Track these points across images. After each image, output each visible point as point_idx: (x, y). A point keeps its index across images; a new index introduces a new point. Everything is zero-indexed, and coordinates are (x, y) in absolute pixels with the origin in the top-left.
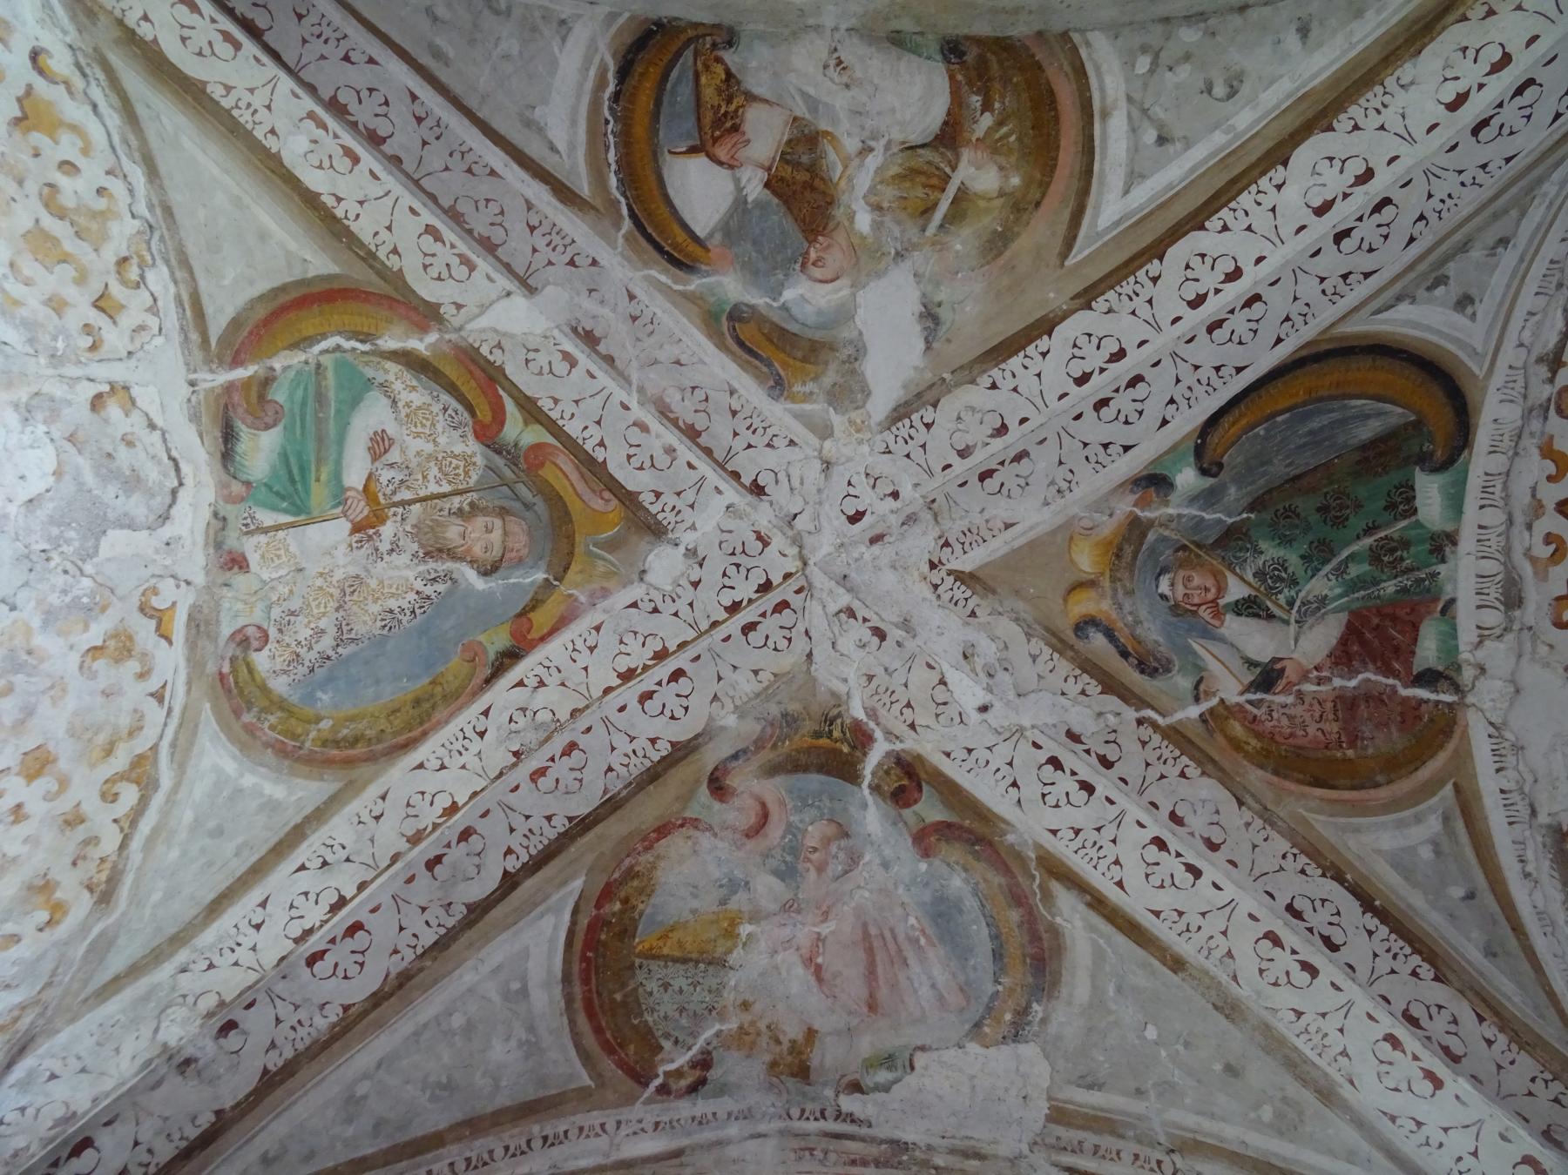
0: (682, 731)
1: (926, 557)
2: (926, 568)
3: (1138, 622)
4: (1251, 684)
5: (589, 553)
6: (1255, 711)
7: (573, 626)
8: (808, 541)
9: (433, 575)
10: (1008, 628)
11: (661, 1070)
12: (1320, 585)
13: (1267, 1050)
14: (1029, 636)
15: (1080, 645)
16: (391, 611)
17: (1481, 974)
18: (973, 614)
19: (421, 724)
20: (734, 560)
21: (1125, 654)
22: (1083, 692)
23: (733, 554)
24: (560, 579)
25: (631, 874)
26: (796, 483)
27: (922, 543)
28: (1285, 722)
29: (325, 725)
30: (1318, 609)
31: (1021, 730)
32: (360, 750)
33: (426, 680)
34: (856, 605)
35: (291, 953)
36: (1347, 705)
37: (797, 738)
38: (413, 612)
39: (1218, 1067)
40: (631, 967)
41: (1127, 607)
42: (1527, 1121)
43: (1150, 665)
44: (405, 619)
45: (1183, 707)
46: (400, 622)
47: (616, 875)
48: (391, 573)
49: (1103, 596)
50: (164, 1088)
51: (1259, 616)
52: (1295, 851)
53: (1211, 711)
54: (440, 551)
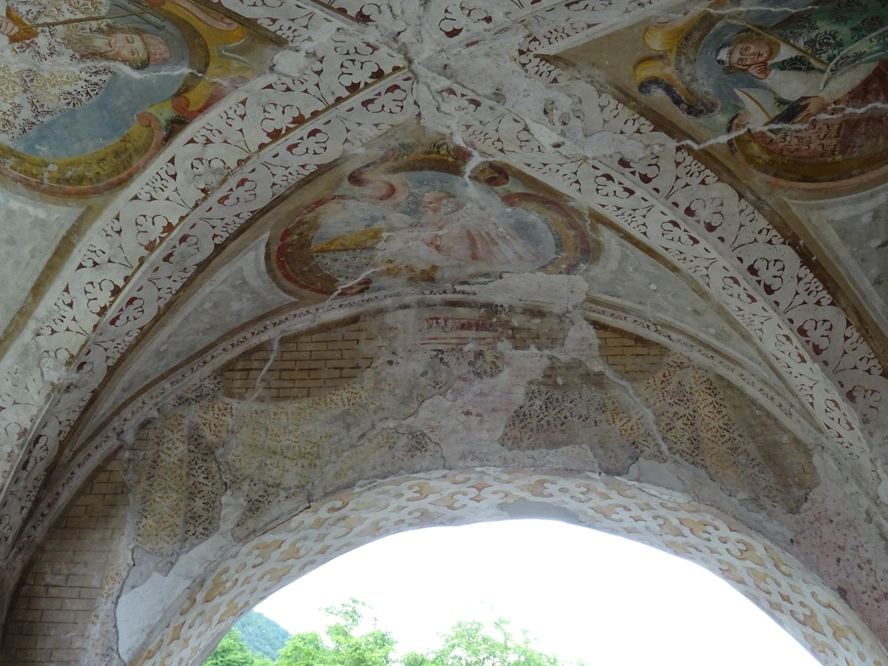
0: (325, 158)
1: (517, 47)
2: (516, 54)
3: (694, 79)
4: (777, 117)
5: (222, 56)
6: (773, 136)
7: (223, 102)
8: (412, 50)
9: (94, 70)
10: (583, 88)
11: (339, 288)
12: (861, 46)
13: (719, 314)
14: (600, 93)
15: (643, 98)
16: (70, 94)
17: (864, 297)
18: (555, 80)
19: (125, 168)
20: (349, 57)
21: (677, 102)
22: (638, 131)
23: (348, 53)
24: (204, 72)
25: (301, 223)
26: (398, 11)
27: (516, 39)
28: (795, 141)
29: (53, 168)
30: (854, 61)
31: (585, 159)
32: (86, 186)
33: (117, 140)
34: (455, 87)
35: (99, 322)
36: (851, 125)
37: (413, 155)
38: (88, 93)
39: (689, 309)
40: (312, 257)
41: (687, 70)
42: (842, 386)
43: (696, 107)
44: (84, 99)
45: (716, 136)
46: (80, 100)
47: (292, 225)
48: (56, 68)
49: (668, 64)
50: (62, 401)
51: (800, 69)
52: (770, 227)
53: (738, 139)
54: (93, 54)
